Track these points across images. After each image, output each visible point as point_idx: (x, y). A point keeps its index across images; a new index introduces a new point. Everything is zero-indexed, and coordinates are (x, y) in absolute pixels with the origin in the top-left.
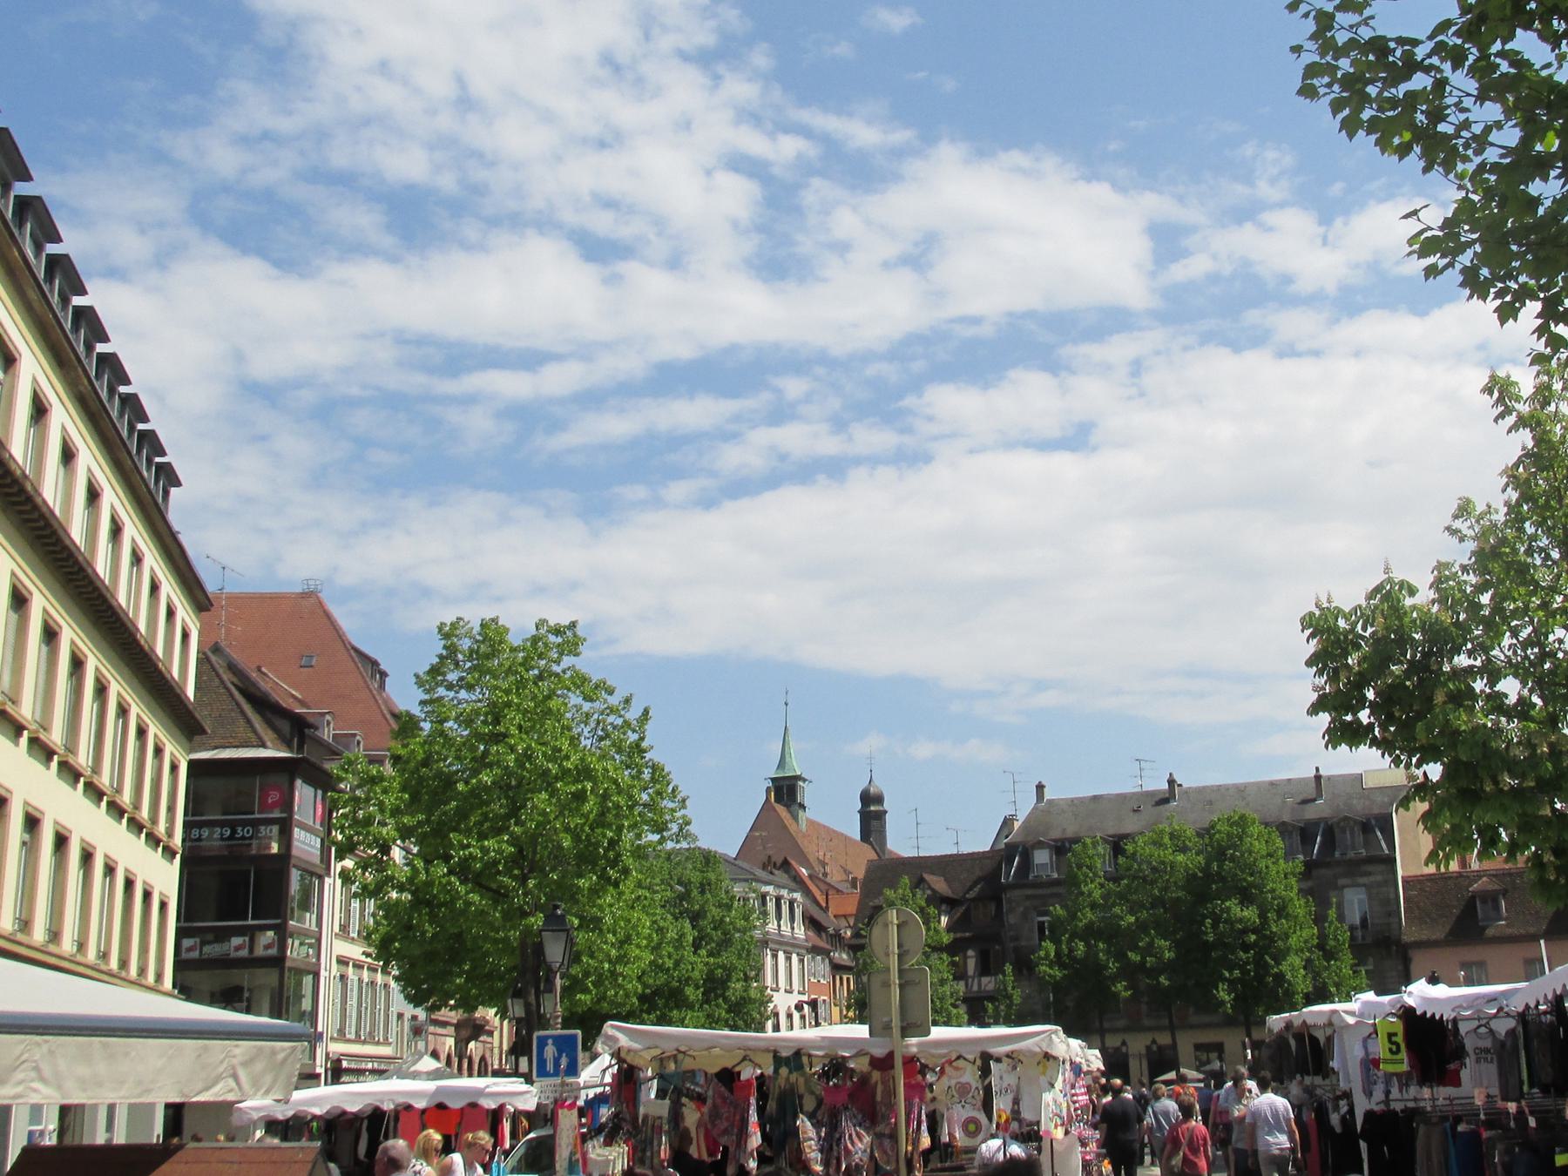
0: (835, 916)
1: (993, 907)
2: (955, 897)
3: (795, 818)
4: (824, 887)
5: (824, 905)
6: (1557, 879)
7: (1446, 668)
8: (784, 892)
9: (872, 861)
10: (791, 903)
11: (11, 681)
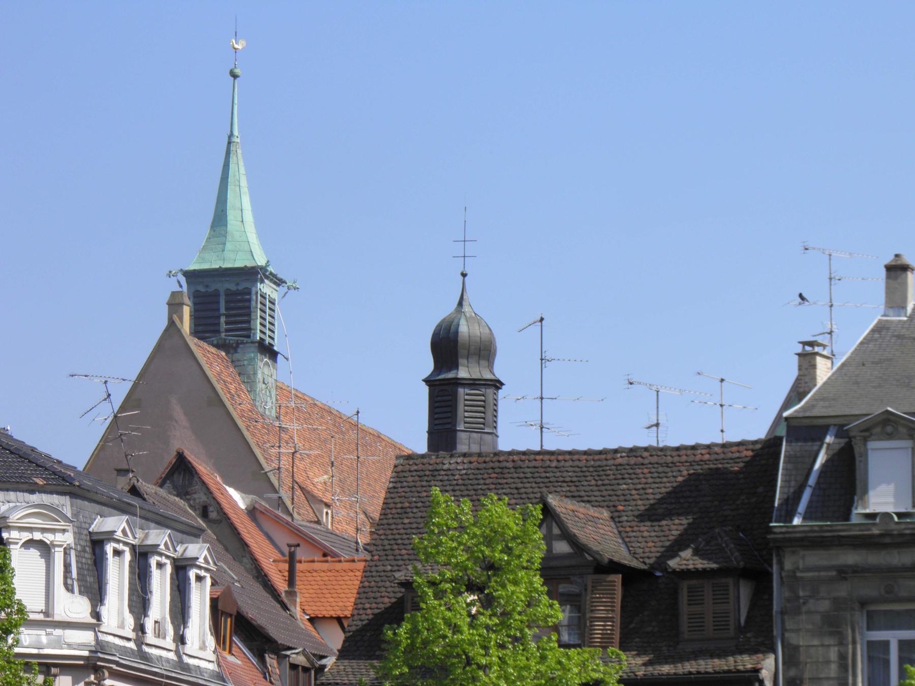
0: (312, 620)
1: (745, 592)
2: (635, 564)
3: (247, 377)
4: (284, 540)
5: (281, 585)
6: (387, 632)
7: (449, 664)
8: (159, 537)
9: (410, 457)
10: (181, 568)
11: (667, 663)
